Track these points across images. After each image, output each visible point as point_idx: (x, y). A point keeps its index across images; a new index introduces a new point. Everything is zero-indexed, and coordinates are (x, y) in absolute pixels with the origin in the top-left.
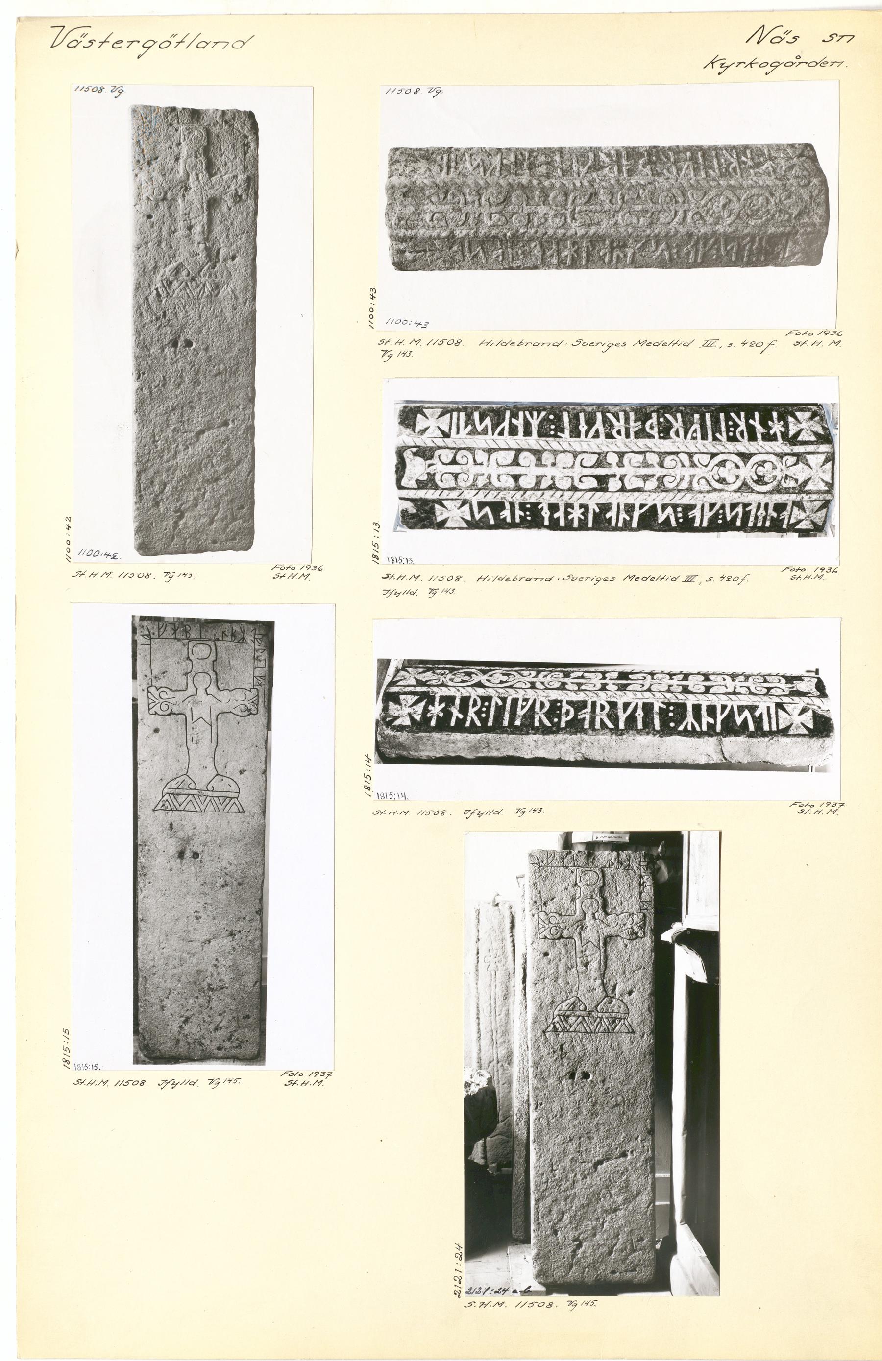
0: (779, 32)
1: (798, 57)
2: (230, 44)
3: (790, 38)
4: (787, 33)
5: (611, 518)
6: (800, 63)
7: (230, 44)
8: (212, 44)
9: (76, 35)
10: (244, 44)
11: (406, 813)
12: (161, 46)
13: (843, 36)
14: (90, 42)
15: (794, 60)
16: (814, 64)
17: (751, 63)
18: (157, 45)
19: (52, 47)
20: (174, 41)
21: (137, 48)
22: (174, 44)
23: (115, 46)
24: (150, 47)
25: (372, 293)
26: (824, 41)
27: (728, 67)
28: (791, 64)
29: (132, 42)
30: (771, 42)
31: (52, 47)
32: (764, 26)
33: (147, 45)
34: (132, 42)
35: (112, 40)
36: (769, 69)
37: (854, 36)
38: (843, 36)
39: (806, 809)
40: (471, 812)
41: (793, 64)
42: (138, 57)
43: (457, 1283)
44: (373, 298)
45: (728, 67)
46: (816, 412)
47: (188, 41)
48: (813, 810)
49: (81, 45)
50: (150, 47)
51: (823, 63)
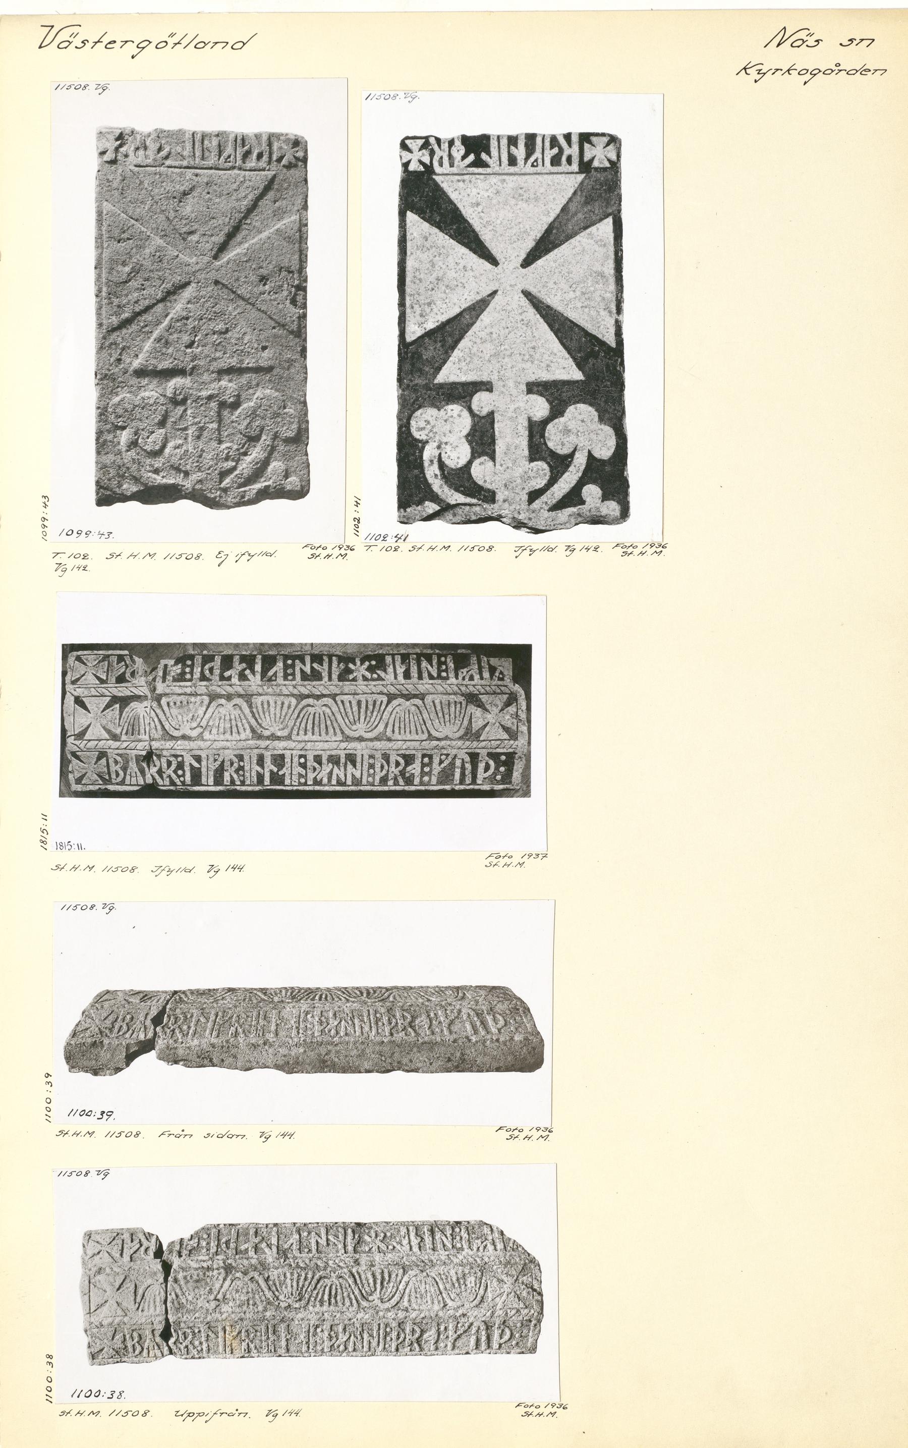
0: (803, 35)
1: (838, 65)
2: (229, 46)
3: (811, 42)
4: (811, 35)
5: (552, 148)
6: (840, 71)
7: (229, 46)
8: (211, 45)
9: (64, 35)
10: (244, 44)
11: (91, 868)
12: (60, 46)
13: (216, 43)
14: (816, 41)
15: (834, 68)
16: (854, 72)
17: (788, 70)
18: (153, 45)
19: (40, 47)
20: (171, 41)
21: (131, 49)
22: (170, 45)
23: (108, 46)
24: (143, 48)
25: (44, 500)
26: (841, 44)
27: (765, 74)
28: (830, 71)
29: (126, 42)
30: (792, 46)
31: (40, 47)
32: (785, 28)
33: (141, 46)
34: (126, 42)
35: (105, 40)
36: (808, 76)
37: (873, 40)
38: (216, 43)
39: (516, 1133)
40: (162, 868)
41: (833, 71)
42: (133, 57)
43: (356, 523)
44: (46, 506)
45: (765, 74)
46: (613, 140)
47: (184, 43)
48: (522, 1135)
49: (72, 46)
50: (143, 48)
51: (864, 71)
